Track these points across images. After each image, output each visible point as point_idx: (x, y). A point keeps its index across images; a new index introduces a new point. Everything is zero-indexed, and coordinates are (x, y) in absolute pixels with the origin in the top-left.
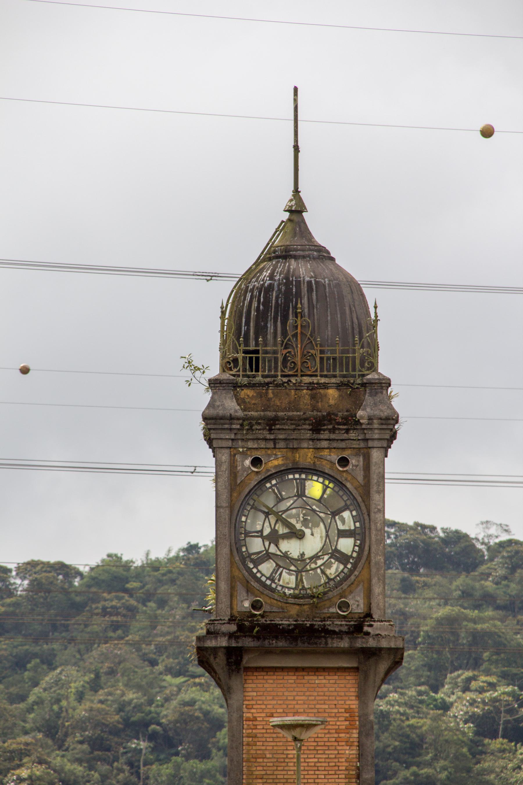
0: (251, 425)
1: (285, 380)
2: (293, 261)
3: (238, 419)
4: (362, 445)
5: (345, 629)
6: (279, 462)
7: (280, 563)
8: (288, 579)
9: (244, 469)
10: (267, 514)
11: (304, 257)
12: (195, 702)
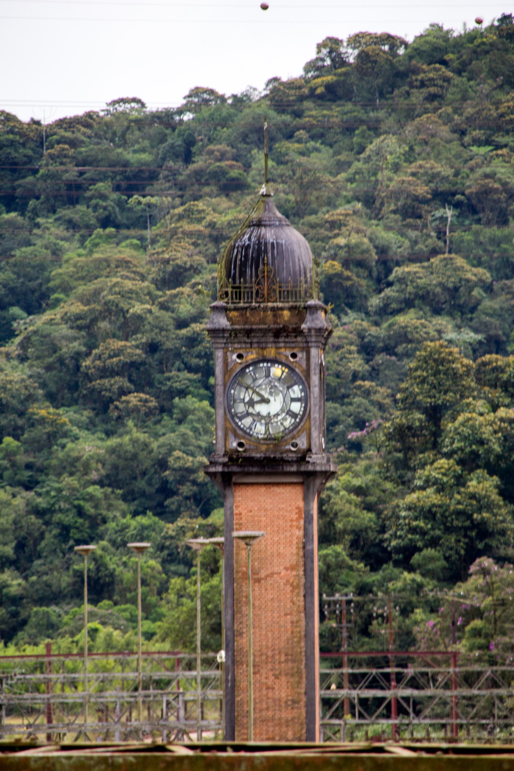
10: (247, 388)
11: (270, 226)
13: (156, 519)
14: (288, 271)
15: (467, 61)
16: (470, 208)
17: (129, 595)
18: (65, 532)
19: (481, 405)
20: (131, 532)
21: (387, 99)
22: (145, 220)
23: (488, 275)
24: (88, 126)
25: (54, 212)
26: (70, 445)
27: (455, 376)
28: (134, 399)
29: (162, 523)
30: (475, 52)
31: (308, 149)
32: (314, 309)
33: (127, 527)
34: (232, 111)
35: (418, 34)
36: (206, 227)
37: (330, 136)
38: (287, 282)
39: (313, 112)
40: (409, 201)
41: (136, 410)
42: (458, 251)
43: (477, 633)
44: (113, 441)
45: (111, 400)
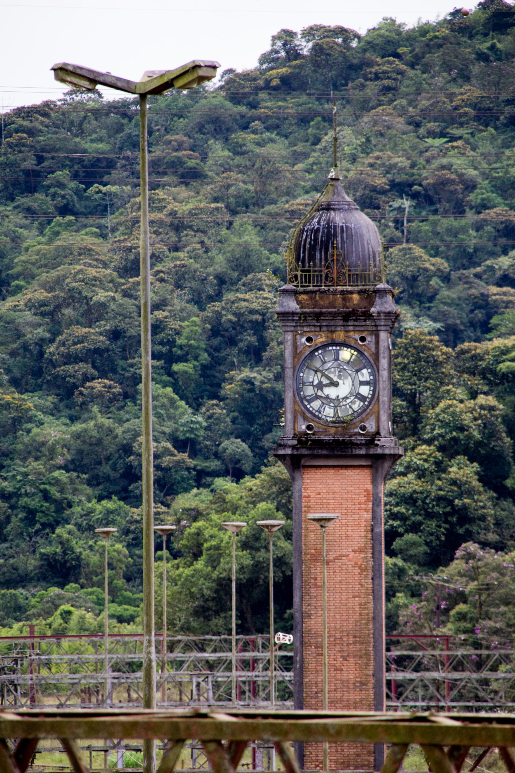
0: (305, 317)
1: (326, 288)
2: (332, 212)
3: (297, 314)
4: (374, 329)
5: (363, 442)
6: (323, 339)
7: (324, 402)
8: (329, 412)
9: (302, 344)
10: (316, 372)
11: (339, 209)
12: (452, 166)
13: (122, 503)
14: (358, 255)
15: (420, 55)
16: (427, 199)
17: (95, 579)
18: (31, 514)
19: (461, 393)
20: (96, 515)
21: (341, 91)
22: (103, 209)
23: (446, 265)
24: (45, 115)
25: (13, 200)
26: (35, 430)
27: (436, 364)
28: (98, 385)
29: (127, 507)
30: (428, 45)
31: (264, 140)
32: (382, 293)
33: (93, 511)
34: (189, 101)
35: (371, 27)
36: (167, 215)
37: (285, 127)
38: (357, 266)
39: (268, 104)
40: (367, 192)
41: (101, 395)
42: (416, 241)
43: (462, 617)
44: (78, 427)
45: (75, 386)
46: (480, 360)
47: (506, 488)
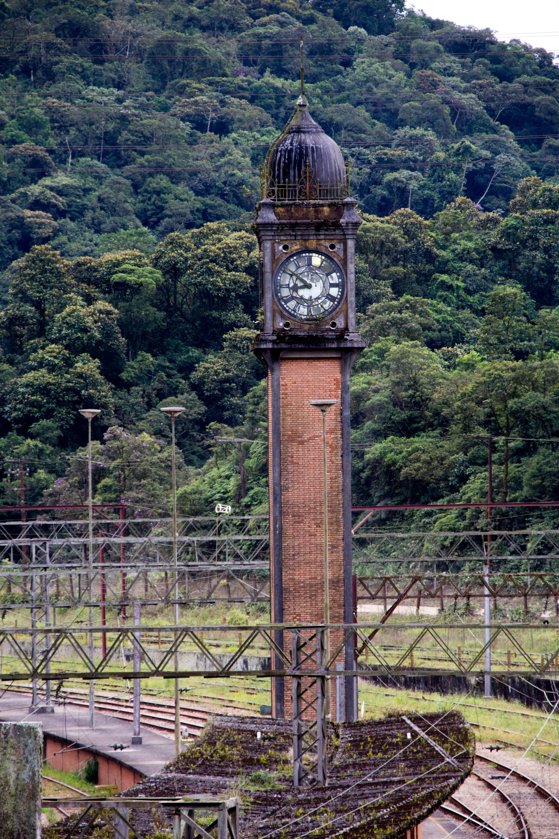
1: (301, 202)
6: (297, 247)
8: (303, 311)
14: (327, 172)
27: (59, 275)
32: (350, 205)
43: (107, 488)
46: (94, 271)
47: (122, 380)
